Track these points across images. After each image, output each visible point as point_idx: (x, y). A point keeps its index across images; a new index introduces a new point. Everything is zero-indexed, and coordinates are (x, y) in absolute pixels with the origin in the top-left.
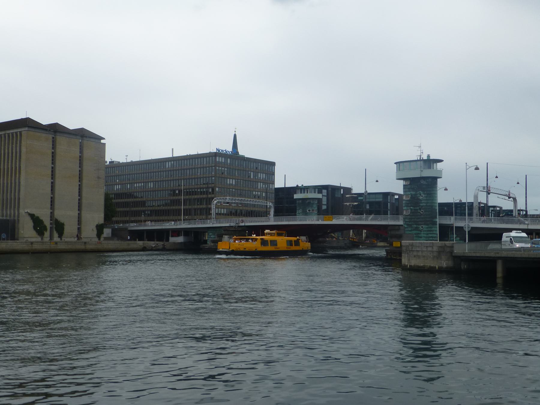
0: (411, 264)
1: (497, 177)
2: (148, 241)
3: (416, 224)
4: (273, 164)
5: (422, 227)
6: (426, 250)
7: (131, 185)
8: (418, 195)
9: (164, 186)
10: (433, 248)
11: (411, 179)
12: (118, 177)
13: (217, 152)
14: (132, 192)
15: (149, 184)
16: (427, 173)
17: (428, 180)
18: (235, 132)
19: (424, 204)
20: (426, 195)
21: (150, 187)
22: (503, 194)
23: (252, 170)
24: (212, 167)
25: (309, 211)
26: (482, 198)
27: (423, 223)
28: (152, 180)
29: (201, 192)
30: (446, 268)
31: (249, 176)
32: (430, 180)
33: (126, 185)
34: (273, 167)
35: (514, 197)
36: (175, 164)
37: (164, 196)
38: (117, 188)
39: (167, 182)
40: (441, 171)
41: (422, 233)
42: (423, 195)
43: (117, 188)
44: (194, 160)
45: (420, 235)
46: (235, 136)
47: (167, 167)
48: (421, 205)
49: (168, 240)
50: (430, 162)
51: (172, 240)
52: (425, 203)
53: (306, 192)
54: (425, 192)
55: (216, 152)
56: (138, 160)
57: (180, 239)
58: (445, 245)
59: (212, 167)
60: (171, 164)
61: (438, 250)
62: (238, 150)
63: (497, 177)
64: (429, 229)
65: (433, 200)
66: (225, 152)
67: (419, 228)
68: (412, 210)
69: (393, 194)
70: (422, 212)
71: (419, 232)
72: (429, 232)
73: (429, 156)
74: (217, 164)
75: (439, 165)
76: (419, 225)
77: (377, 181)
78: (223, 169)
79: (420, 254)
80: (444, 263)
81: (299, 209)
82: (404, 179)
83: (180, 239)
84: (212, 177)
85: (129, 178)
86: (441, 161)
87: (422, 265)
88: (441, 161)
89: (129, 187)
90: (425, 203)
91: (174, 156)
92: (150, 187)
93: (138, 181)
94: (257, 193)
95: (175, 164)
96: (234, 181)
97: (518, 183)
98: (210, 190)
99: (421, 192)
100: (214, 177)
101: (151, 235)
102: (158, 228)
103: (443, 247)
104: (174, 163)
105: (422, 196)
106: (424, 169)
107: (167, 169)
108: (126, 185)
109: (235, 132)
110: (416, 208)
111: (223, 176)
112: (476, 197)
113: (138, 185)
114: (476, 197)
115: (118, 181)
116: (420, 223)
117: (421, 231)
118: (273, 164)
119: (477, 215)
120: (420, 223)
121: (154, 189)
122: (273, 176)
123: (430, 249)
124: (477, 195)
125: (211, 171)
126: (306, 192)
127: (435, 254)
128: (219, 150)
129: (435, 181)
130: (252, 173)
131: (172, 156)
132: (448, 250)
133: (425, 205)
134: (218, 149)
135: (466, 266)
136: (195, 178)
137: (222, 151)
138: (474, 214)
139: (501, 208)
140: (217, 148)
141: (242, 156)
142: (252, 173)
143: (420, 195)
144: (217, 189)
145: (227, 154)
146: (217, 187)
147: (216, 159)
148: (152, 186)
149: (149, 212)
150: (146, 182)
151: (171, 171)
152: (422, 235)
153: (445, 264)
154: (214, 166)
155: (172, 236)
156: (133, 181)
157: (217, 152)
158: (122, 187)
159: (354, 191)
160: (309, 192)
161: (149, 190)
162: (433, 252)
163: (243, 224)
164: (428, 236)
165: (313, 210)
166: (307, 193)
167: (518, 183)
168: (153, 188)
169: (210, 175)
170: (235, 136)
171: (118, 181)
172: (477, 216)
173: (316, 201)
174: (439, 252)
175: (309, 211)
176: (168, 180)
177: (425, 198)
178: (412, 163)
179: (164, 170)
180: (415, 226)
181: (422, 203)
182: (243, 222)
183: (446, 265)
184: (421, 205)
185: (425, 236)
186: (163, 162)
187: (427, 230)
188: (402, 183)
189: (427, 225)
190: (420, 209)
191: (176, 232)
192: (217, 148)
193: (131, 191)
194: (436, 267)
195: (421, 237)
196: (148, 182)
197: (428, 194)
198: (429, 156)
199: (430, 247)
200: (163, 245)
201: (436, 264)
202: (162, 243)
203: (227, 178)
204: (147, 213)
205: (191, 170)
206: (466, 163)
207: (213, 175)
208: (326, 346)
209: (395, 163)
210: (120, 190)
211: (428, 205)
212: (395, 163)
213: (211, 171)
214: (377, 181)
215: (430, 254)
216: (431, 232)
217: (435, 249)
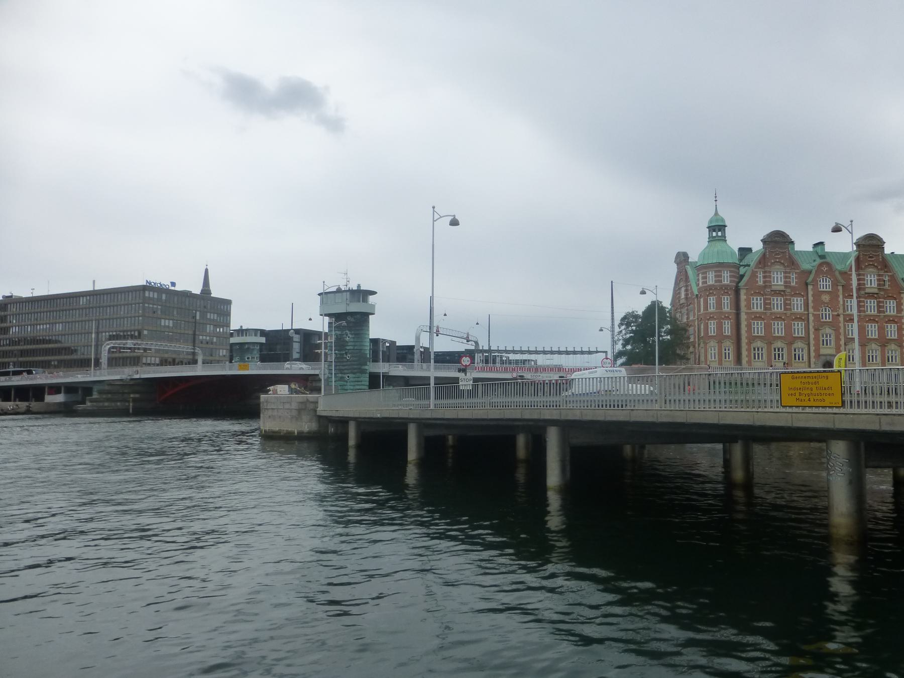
0: (266, 428)
1: (445, 315)
2: (19, 401)
3: (341, 373)
4: (228, 303)
5: (348, 377)
6: (282, 408)
7: (20, 327)
8: (344, 336)
9: (77, 329)
10: (291, 405)
11: (337, 315)
12: (15, 316)
13: (148, 284)
14: (36, 337)
15: (57, 325)
16: (355, 307)
17: (356, 317)
18: (207, 266)
19: (351, 347)
20: (353, 336)
21: (57, 330)
22: (459, 336)
23: (199, 309)
24: (139, 304)
25: (248, 358)
26: (425, 342)
27: (350, 371)
28: (61, 321)
29: (125, 336)
30: (309, 432)
31: (194, 317)
32: (358, 316)
33: (26, 327)
34: (229, 306)
35: (476, 340)
36: (92, 300)
37: (76, 341)
38: (14, 331)
39: (80, 323)
40: (373, 306)
41: (348, 384)
42: (350, 336)
43: (14, 331)
44: (116, 295)
45: (346, 387)
46: (207, 271)
47: (81, 303)
48: (348, 348)
49: (42, 399)
50: (362, 294)
51: (50, 399)
52: (352, 346)
53: (244, 335)
54: (353, 332)
55: (145, 284)
56: (47, 294)
57: (60, 398)
58: (307, 400)
59: (139, 304)
60: (86, 300)
61: (297, 408)
62: (209, 288)
63: (445, 315)
64: (357, 379)
65: (362, 342)
66: (159, 285)
67: (344, 377)
68: (337, 355)
69: (384, 341)
70: (349, 357)
71: (345, 383)
72: (357, 383)
73: (359, 286)
74: (146, 300)
75: (371, 299)
76: (345, 374)
77: (310, 319)
78: (155, 306)
79: (275, 413)
80: (305, 425)
81: (236, 356)
82: (329, 315)
83: (60, 398)
84: (138, 317)
85: (36, 317)
86: (374, 293)
87: (277, 429)
88: (374, 293)
89: (29, 330)
90: (352, 346)
91: (96, 289)
92: (57, 330)
93: (41, 322)
94: (204, 337)
95: (92, 300)
96: (171, 322)
97: (477, 324)
98: (136, 334)
99: (347, 331)
100: (141, 316)
101: (23, 393)
102: (61, 382)
103: (305, 403)
104: (90, 299)
105: (349, 337)
106: (351, 302)
107: (81, 307)
108: (26, 327)
109: (207, 266)
110: (342, 352)
111: (155, 315)
112: (418, 339)
113: (41, 327)
114: (418, 339)
115: (14, 321)
116: (346, 371)
117: (347, 382)
118: (228, 303)
119: (419, 360)
120: (346, 371)
121: (63, 333)
122: (228, 317)
123: (287, 406)
124: (419, 336)
125: (137, 309)
126: (244, 335)
127: (294, 413)
128: (150, 283)
129: (366, 317)
130: (198, 313)
131: (92, 289)
132: (311, 406)
133: (353, 348)
134: (149, 281)
135: (333, 429)
136: (116, 318)
137: (155, 284)
138: (416, 360)
139: (393, 343)
140: (147, 281)
141: (188, 291)
142: (198, 313)
143: (347, 335)
144: (145, 332)
145: (163, 288)
146: (146, 330)
147: (144, 294)
148: (60, 329)
149: (56, 363)
150: (52, 324)
151: (86, 308)
152: (349, 387)
153: (306, 427)
154: (142, 303)
155: (49, 394)
156: (35, 322)
157: (148, 284)
158: (20, 330)
159: (397, 344)
160: (248, 335)
161: (57, 333)
162: (291, 410)
163: (137, 376)
164: (355, 388)
165: (253, 358)
166: (246, 336)
167: (477, 324)
168: (62, 331)
169: (137, 315)
170: (207, 271)
171: (14, 321)
172: (419, 363)
173: (257, 347)
174: (299, 411)
175: (248, 358)
176: (82, 321)
177: (352, 340)
178: (329, 295)
179: (77, 307)
180: (340, 375)
181: (348, 346)
182: (138, 373)
183: (308, 428)
184: (348, 348)
185: (352, 388)
186: (76, 297)
187: (354, 380)
188: (327, 319)
189: (354, 373)
190: (346, 354)
191: (55, 389)
192: (147, 281)
193: (32, 335)
194: (294, 433)
195: (347, 390)
196: (56, 323)
197: (355, 334)
198: (359, 286)
199: (288, 403)
200: (27, 406)
201: (294, 427)
202: (26, 404)
203: (161, 319)
204: (53, 363)
205: (120, 307)
206: (324, 282)
207: (140, 315)
208: (81, 564)
209: (319, 294)
210: (17, 333)
211: (355, 348)
212: (319, 294)
213: (137, 309)
214: (310, 319)
215: (288, 413)
216: (359, 383)
217: (294, 406)
